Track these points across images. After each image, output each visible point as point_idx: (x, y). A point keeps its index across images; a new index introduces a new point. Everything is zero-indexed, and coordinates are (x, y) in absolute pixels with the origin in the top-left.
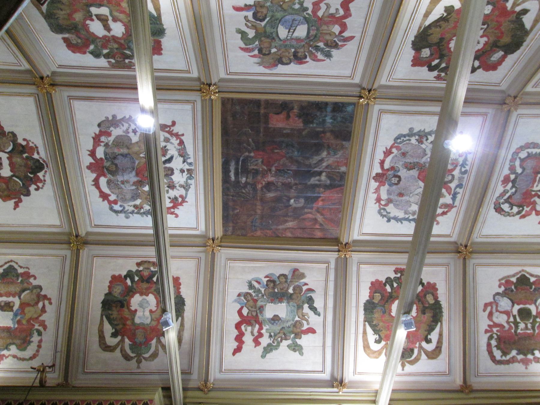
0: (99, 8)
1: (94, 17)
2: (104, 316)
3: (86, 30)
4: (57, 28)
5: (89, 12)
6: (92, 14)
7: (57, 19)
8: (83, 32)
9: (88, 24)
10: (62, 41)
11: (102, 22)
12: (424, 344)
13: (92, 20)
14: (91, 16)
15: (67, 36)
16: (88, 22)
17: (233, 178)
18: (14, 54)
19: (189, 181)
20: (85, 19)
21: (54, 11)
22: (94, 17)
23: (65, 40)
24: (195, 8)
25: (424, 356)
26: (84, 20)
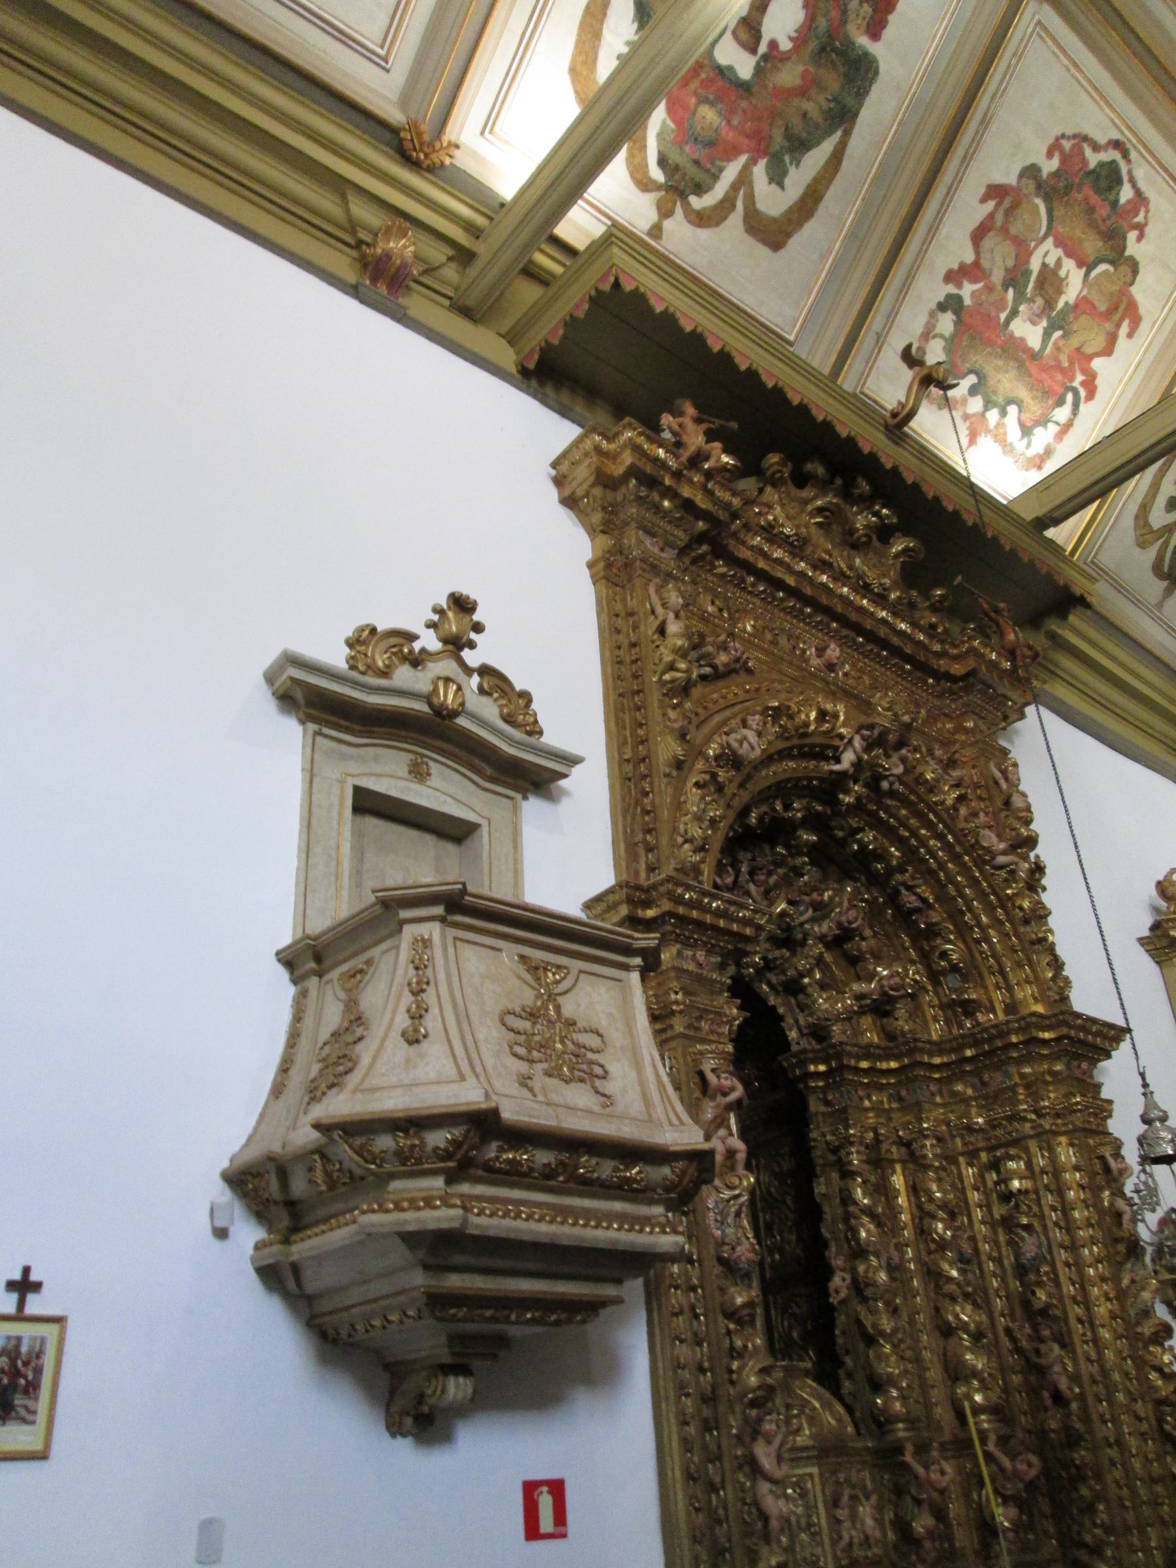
0: (730, 68)
1: (763, 48)
2: (457, 1132)
3: (810, 27)
4: (859, 72)
5: (759, 71)
6: (758, 63)
7: (835, 100)
8: (822, 23)
9: (791, 39)
10: (888, 33)
11: (760, 23)
12: (759, 172)
13: (773, 44)
14: (765, 57)
15: (863, 41)
16: (785, 45)
17: (1067, 1154)
18: (1018, 55)
19: (545, 1489)
20: (785, 57)
21: (821, 121)
22: (763, 48)
23: (875, 30)
24: (526, 194)
25: (736, 218)
26: (788, 59)
